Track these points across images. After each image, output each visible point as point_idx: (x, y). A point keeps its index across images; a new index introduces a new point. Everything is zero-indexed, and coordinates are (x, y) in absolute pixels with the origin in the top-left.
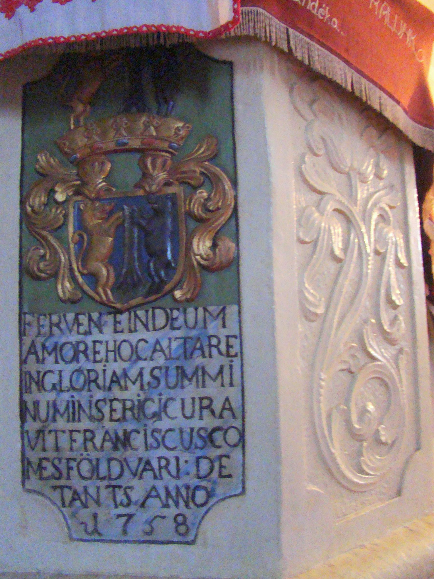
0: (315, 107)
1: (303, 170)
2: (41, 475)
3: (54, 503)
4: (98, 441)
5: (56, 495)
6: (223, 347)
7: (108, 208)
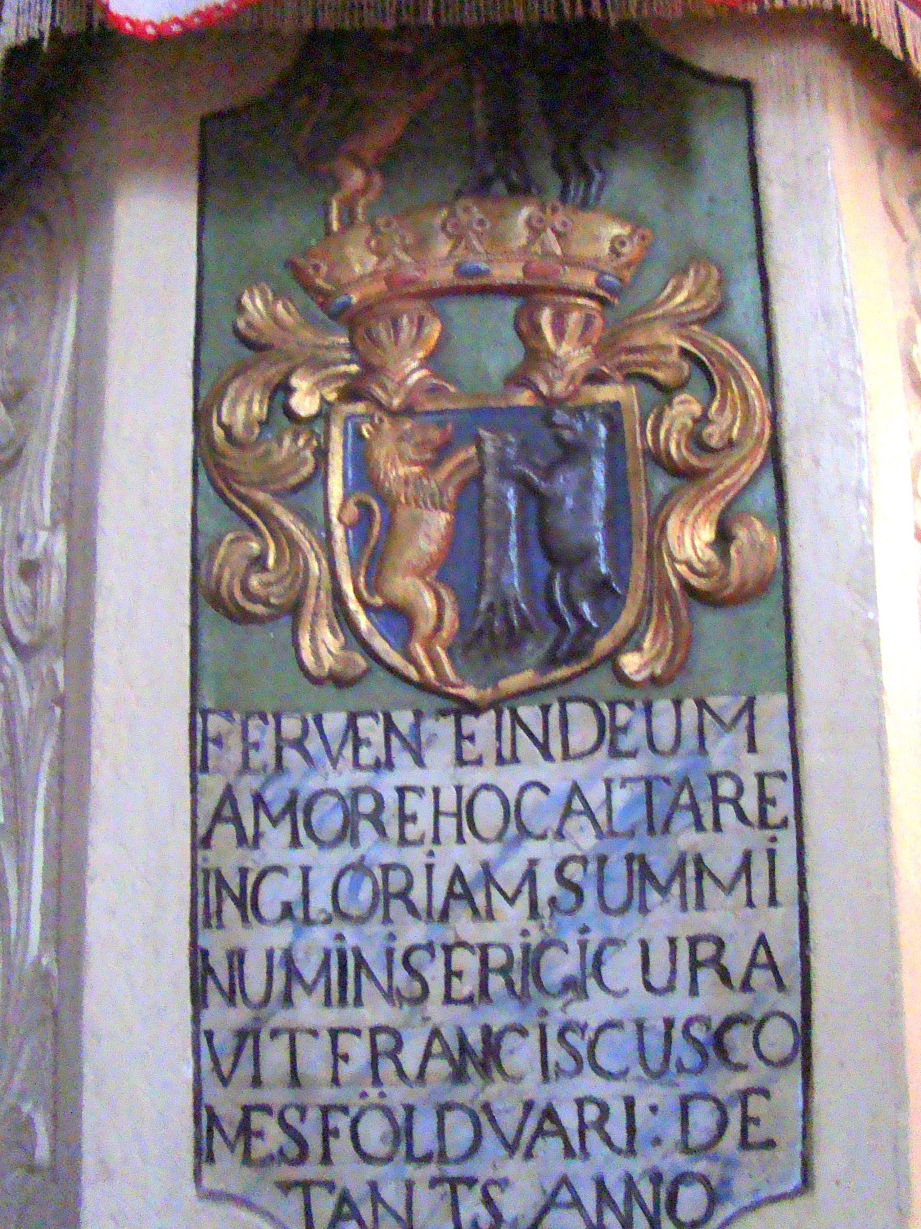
2: (247, 1151)
4: (411, 1059)
6: (750, 803)
7: (435, 435)
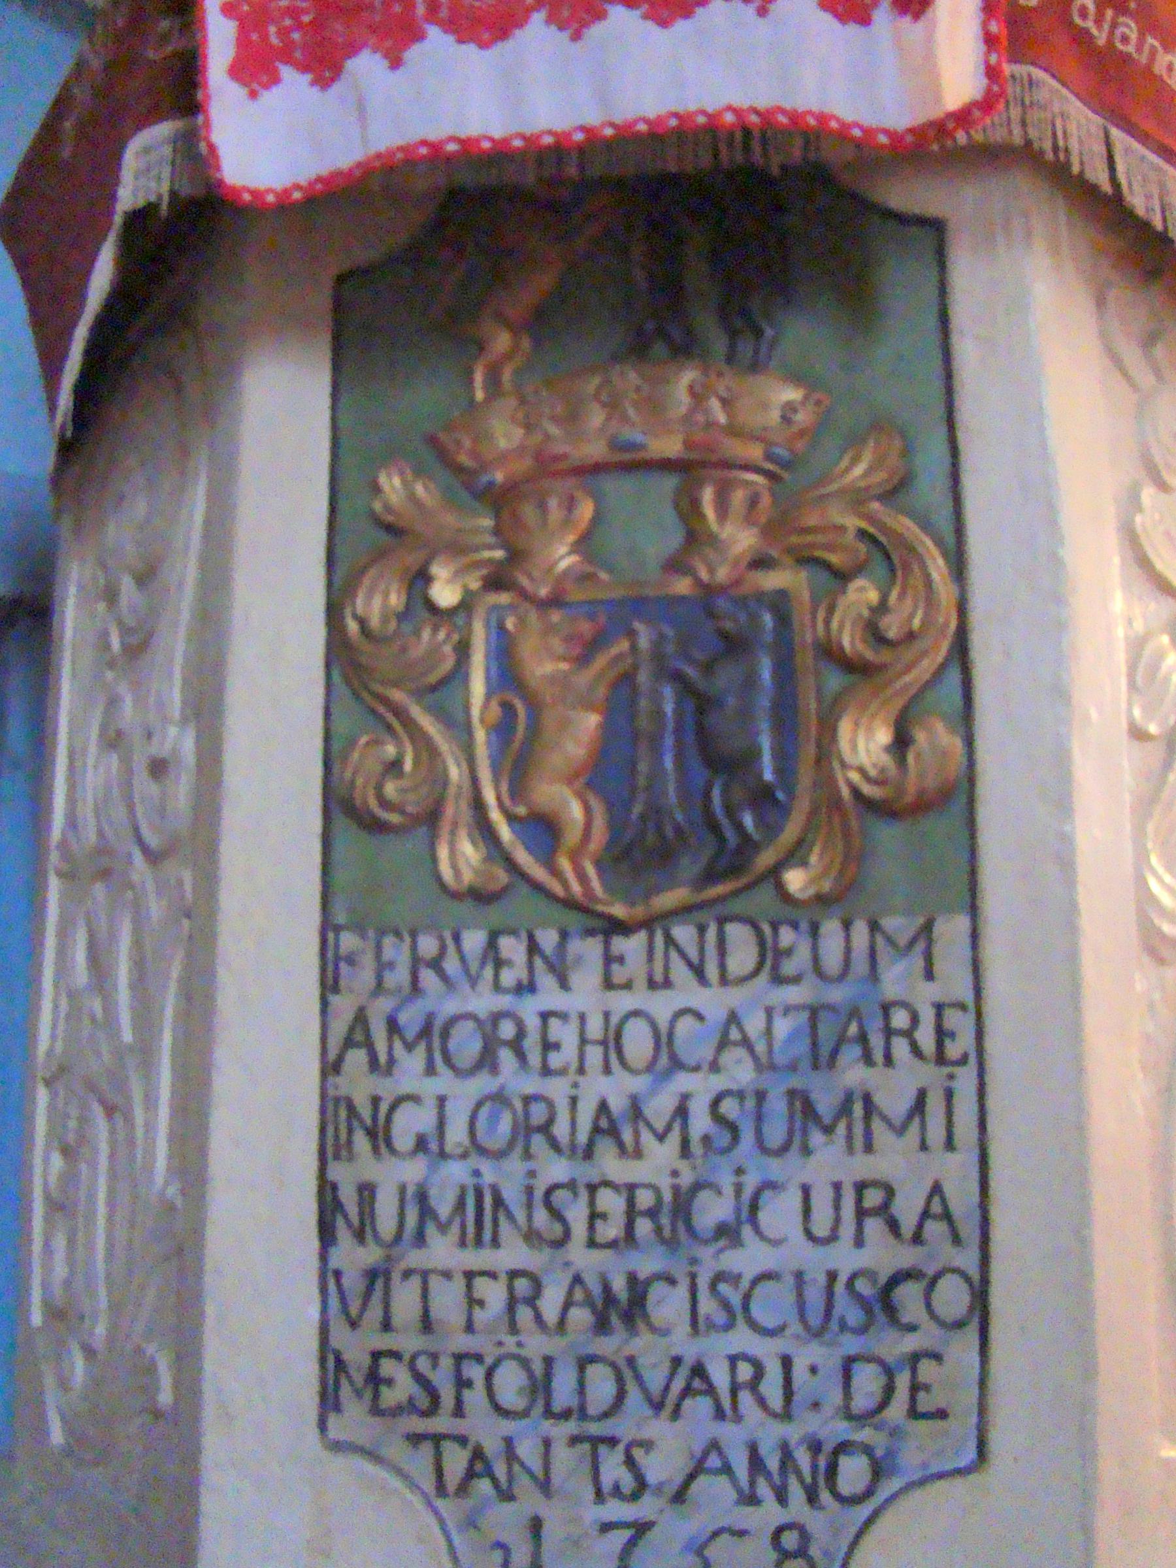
0: (1158, 351)
1: (1139, 529)
3: (415, 1487)
4: (550, 1305)
5: (420, 1463)
6: (926, 1038)
7: (586, 628)
